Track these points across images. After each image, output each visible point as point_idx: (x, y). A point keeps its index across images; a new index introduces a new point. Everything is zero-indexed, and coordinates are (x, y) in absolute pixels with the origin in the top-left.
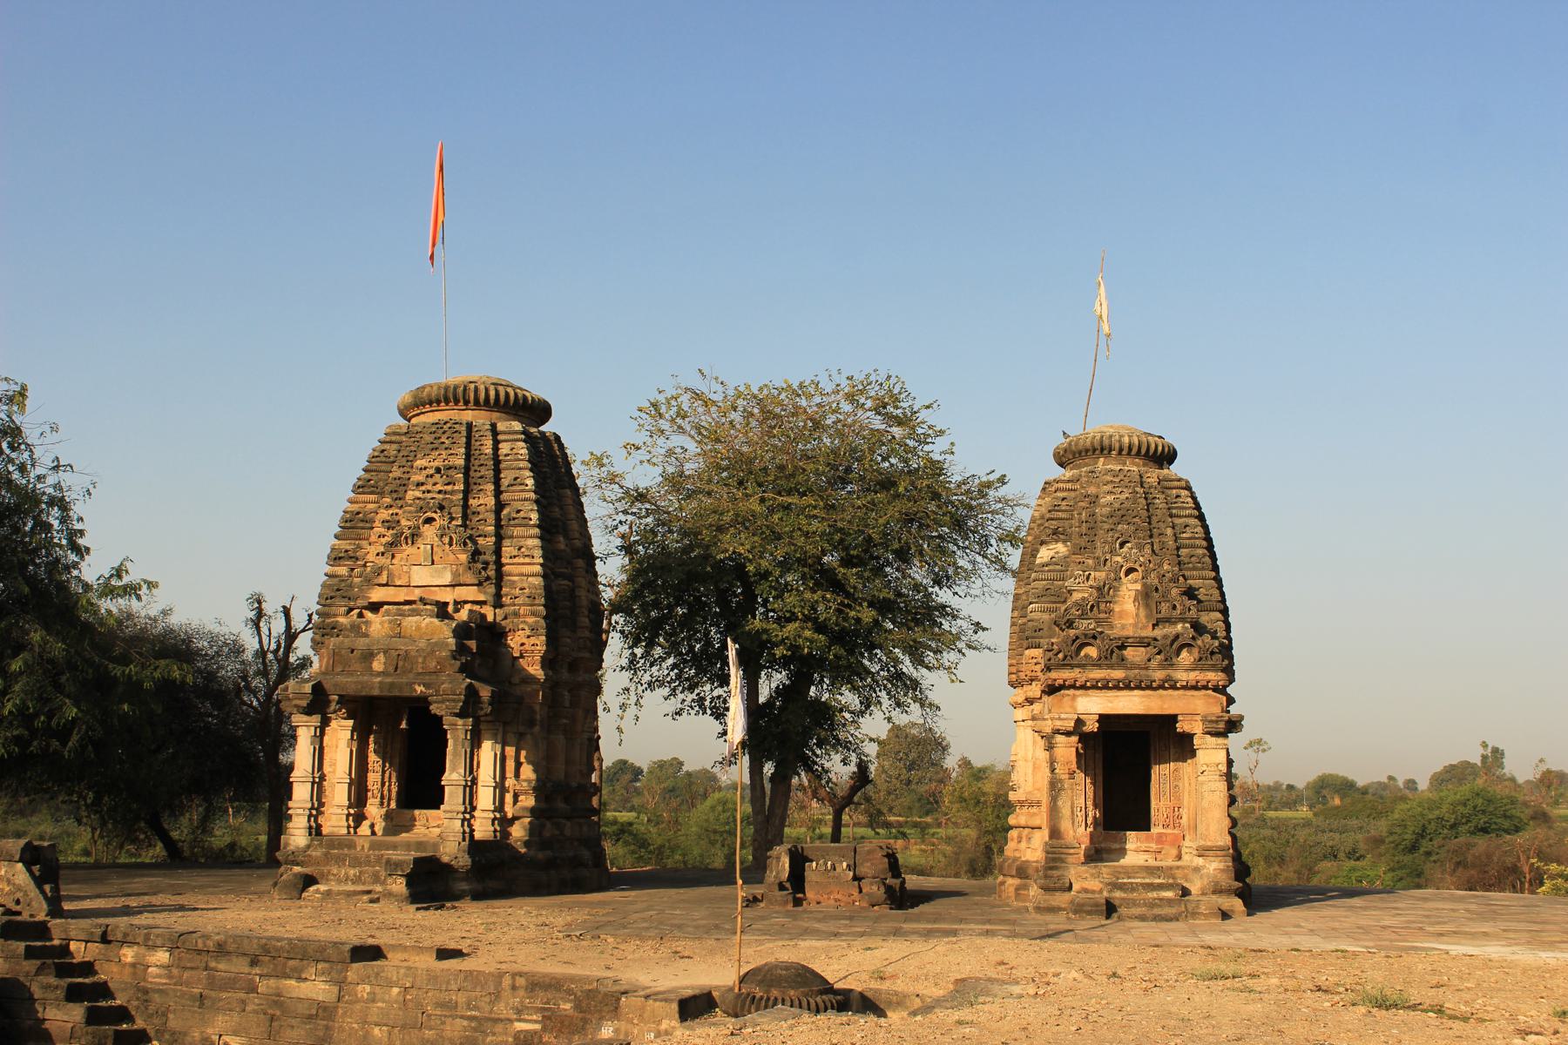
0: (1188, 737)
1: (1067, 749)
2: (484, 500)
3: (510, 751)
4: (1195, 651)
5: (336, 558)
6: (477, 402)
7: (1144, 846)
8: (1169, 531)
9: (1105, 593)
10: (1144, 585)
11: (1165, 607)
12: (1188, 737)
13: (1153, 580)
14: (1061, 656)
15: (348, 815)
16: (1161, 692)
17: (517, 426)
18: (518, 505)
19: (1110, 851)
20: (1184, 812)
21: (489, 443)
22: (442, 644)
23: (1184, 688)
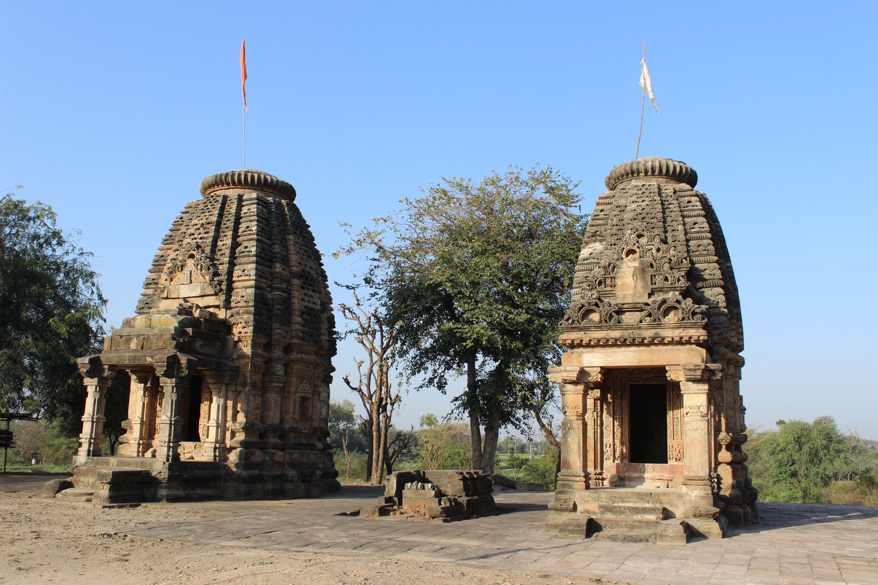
3: (230, 403)
4: (680, 311)
5: (147, 285)
6: (234, 184)
7: (658, 475)
8: (681, 228)
9: (611, 269)
10: (641, 262)
11: (659, 280)
14: (570, 321)
15: (215, 448)
16: (653, 347)
17: (254, 195)
18: (245, 244)
19: (631, 479)
21: (234, 206)
23: (672, 343)
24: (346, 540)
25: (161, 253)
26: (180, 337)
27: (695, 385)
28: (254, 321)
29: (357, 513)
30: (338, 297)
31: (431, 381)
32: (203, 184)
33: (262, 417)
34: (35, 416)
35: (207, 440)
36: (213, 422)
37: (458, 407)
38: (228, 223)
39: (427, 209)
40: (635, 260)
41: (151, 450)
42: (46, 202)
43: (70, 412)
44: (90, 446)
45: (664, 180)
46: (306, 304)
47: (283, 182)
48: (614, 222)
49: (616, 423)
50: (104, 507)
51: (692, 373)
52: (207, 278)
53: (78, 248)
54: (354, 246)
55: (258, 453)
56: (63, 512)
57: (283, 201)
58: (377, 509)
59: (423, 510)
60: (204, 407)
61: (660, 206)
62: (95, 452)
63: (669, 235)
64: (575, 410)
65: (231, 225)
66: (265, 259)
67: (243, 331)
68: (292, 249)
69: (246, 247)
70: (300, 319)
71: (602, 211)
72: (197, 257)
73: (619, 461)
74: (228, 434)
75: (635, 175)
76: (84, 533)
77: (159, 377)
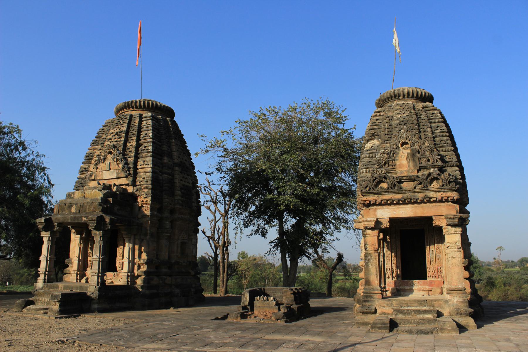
0: (440, 228)
1: (373, 237)
2: (132, 143)
3: (137, 247)
5: (81, 172)
8: (429, 129)
9: (392, 155)
10: (412, 150)
11: (423, 161)
12: (440, 228)
13: (416, 147)
14: (368, 189)
15: (128, 276)
16: (423, 205)
17: (150, 114)
18: (145, 145)
19: (405, 290)
20: (443, 270)
22: (98, 200)
23: (436, 201)
24: (230, 340)
25: (90, 151)
26: (104, 204)
27: (453, 228)
28: (152, 193)
29: (225, 318)
30: (201, 180)
31: (257, 231)
32: (117, 108)
33: (157, 255)
34: (8, 257)
35: (122, 271)
36: (126, 259)
37: (274, 247)
38: (134, 132)
39: (250, 127)
40: (407, 149)
41: (85, 278)
42: (15, 123)
43: (31, 254)
44: (45, 276)
45: (415, 101)
46: (184, 183)
47: (167, 107)
48: (386, 127)
49: (393, 255)
50: (56, 318)
51: (452, 220)
52: (121, 166)
53: (35, 152)
54: (209, 149)
55: (156, 278)
56: (28, 322)
57: (167, 118)
58: (239, 315)
59: (269, 315)
60: (119, 250)
61: (415, 116)
62: (48, 281)
63: (422, 134)
64: (373, 247)
65: (135, 133)
66: (157, 155)
67: (145, 201)
68: (174, 148)
69: (146, 147)
70: (180, 192)
71: (377, 120)
72: (114, 153)
73: (396, 279)
74: (136, 267)
75: (397, 97)
76: (44, 339)
77: (91, 230)
